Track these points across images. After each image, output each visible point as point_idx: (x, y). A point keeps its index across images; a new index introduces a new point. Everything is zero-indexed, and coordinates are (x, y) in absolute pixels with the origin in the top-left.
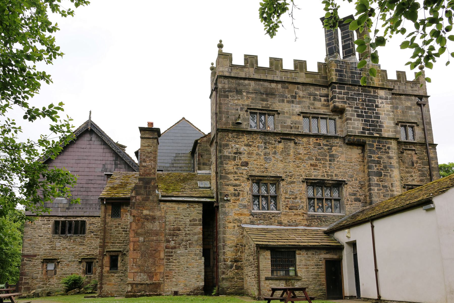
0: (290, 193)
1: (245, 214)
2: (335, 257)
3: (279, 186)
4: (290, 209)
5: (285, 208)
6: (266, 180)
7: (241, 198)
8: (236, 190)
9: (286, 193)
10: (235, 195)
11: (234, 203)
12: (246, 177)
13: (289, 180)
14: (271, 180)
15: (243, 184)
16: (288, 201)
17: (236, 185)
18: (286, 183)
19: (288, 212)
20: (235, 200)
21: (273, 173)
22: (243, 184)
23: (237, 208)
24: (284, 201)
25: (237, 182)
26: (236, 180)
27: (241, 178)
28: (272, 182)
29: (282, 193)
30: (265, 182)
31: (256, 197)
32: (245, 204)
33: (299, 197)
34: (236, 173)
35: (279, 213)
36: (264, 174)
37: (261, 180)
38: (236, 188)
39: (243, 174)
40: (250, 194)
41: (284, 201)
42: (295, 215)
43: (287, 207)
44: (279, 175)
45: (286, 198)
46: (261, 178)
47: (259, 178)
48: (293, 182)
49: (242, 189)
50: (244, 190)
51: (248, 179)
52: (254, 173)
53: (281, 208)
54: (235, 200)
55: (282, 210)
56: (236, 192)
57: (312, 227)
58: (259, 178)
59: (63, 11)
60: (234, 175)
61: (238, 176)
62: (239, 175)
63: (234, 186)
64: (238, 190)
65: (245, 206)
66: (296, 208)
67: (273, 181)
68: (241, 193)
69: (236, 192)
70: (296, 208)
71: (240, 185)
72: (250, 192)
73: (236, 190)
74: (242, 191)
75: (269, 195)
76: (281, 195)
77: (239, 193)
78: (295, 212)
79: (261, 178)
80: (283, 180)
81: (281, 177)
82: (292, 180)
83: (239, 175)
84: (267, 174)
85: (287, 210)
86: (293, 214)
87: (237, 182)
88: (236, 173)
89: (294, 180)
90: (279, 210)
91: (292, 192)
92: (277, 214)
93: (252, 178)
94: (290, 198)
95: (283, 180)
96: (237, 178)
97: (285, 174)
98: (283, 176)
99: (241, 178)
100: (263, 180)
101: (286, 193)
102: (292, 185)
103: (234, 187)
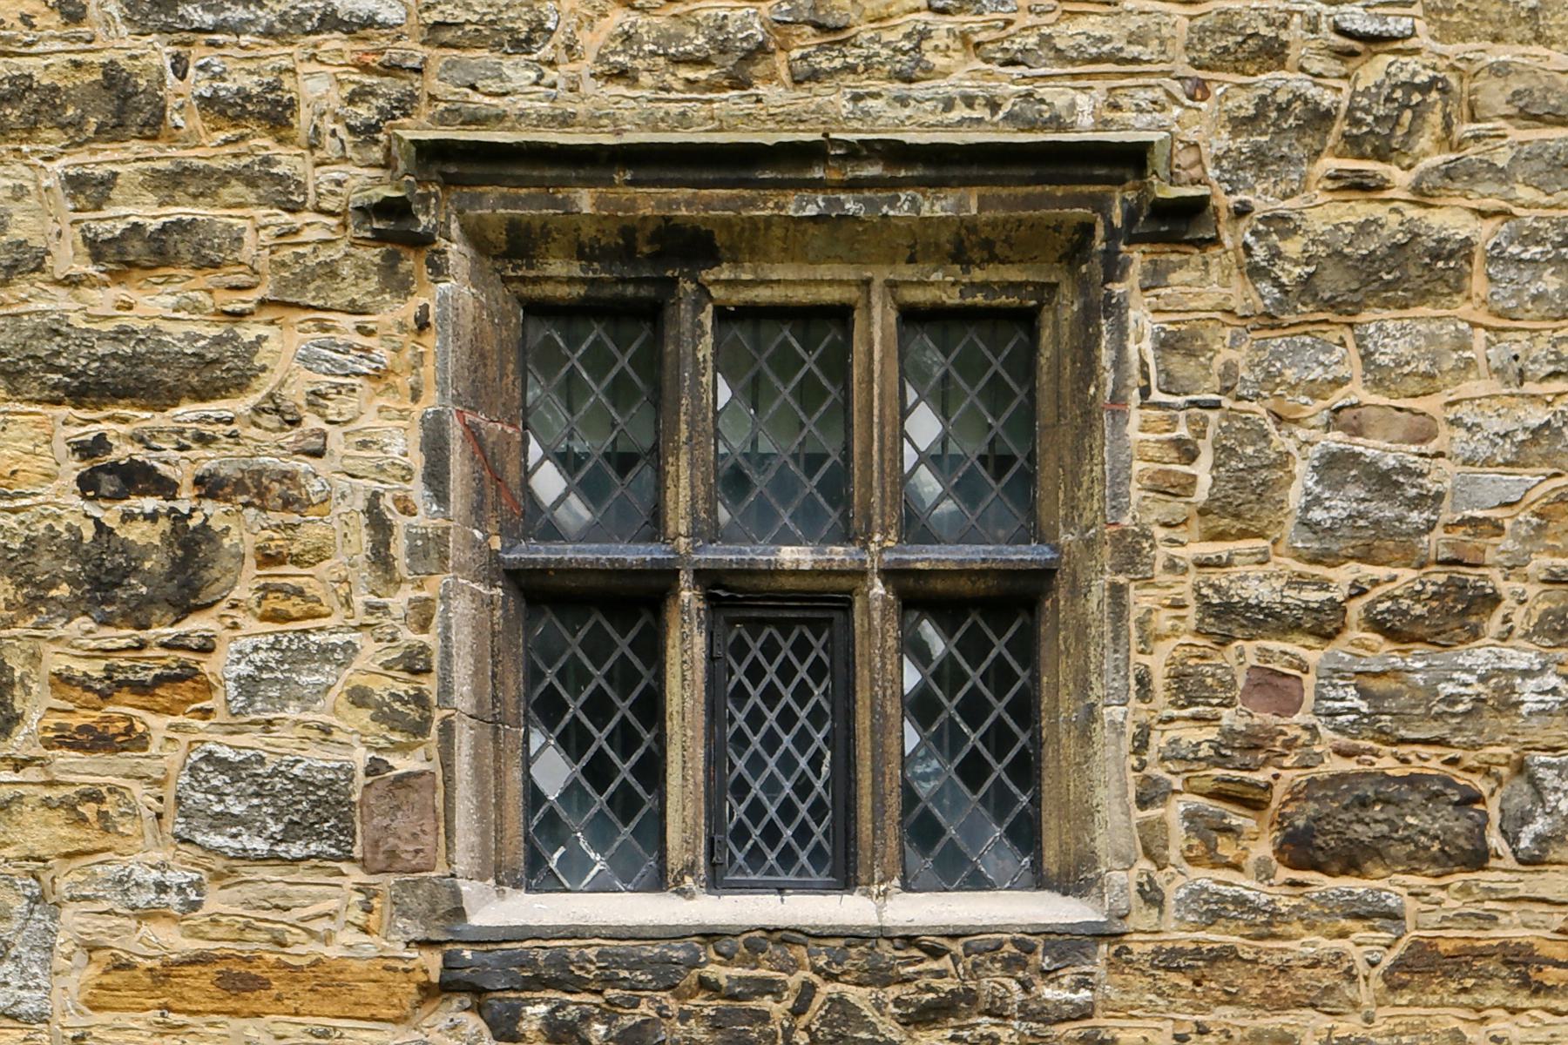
0: (1339, 507)
1: (325, 981)
2: (676, 856)
3: (1088, 369)
4: (1300, 849)
5: (1207, 830)
6: (795, 238)
7: (235, 639)
8: (137, 478)
9: (1240, 507)
10: (103, 581)
11: (94, 741)
12: (362, 181)
13: (1327, 215)
14: (920, 244)
15: (283, 350)
16: (1273, 686)
17: (133, 378)
18: (1244, 295)
19: (1269, 923)
20: (113, 685)
21: (962, 74)
22: (283, 350)
23: (146, 857)
24: (1186, 686)
25: (162, 309)
26: (122, 256)
27: (251, 223)
28: (941, 286)
29: (1141, 508)
30: (785, 281)
31: (579, 634)
32: (318, 759)
33: (1523, 599)
34: (125, 106)
35: (1069, 944)
36: (770, 111)
37: (692, 246)
38: (123, 429)
39: (276, 114)
40: (430, 550)
41: (1186, 686)
42: (1420, 966)
43: (1252, 800)
44: (1083, 114)
45: (1227, 617)
46: (683, 202)
47: (650, 201)
48: (1423, 270)
49: (270, 450)
50: (317, 476)
51: (393, 227)
52: (523, 100)
53: (1114, 821)
54: (113, 685)
55: (1122, 879)
56: (140, 526)
57: (714, 713)
58: (650, 201)
59: (177, 894)
60: (99, 160)
61: (172, 181)
62: (209, 147)
63: (85, 391)
64: (181, 468)
65: (318, 816)
66: (1444, 821)
67: (963, 246)
68: (240, 529)
69: (140, 526)
70: (1444, 821)
71: (216, 374)
72: (426, 518)
73: (137, 478)
74: (251, 488)
75: (883, 548)
76: (1131, 551)
77: (192, 547)
78: (1430, 904)
79: (683, 202)
80: (1181, 224)
81: (1134, 157)
82: (1390, 218)
83: (209, 147)
84: (834, 99)
85: (1254, 869)
86: (1365, 946)
87: (162, 309)
88: (125, 106)
89: (1450, 220)
90: (1074, 879)
91: (1384, 481)
92: (1021, 951)
93: (495, 204)
94: (1324, 624)
95: (1181, 224)
96: (150, 213)
97: (1235, 92)
98: (1193, 134)
99: (251, 223)
100: (750, 240)
101: (1240, 507)
102: (1395, 331)
103: (75, 422)
